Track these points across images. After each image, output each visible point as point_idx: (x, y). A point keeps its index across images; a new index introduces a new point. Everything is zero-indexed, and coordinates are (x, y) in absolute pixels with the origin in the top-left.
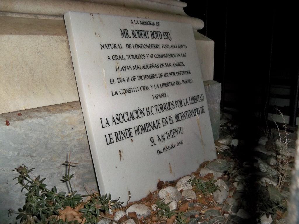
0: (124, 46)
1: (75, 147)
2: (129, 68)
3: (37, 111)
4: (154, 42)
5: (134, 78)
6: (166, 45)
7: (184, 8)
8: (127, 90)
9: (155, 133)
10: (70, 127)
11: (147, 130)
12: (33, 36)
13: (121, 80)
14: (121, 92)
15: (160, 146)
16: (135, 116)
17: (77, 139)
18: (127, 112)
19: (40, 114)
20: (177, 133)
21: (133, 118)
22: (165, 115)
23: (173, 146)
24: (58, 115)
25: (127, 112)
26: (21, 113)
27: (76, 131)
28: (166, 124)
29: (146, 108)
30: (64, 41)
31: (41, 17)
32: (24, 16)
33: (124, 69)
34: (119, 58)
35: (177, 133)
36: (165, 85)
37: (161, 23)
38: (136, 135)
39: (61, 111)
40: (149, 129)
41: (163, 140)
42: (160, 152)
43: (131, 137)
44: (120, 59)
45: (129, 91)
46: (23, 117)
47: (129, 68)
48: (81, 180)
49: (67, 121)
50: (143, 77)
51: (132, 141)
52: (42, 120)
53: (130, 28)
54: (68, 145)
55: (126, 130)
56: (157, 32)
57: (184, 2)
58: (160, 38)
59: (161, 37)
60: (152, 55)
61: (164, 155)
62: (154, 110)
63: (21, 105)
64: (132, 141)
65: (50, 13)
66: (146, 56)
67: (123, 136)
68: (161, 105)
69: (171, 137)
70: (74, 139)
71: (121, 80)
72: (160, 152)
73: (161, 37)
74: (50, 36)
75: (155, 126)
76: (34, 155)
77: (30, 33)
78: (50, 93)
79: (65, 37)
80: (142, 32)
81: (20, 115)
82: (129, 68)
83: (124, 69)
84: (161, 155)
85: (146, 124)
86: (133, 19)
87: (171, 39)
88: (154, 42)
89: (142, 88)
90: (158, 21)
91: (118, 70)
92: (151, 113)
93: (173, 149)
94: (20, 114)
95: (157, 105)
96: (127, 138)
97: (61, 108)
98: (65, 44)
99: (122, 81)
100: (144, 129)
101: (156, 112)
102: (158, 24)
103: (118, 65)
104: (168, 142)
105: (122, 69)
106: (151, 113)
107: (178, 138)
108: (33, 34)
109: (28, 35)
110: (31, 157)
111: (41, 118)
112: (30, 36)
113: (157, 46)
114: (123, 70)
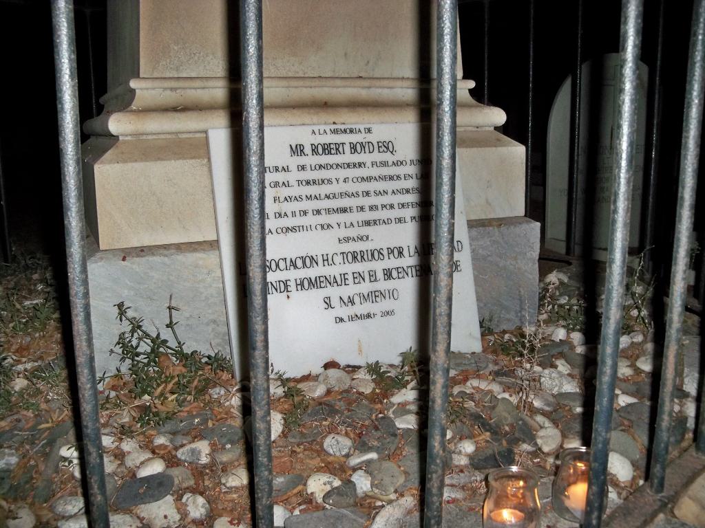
0: (293, 168)
1: (212, 296)
2: (298, 199)
3: (165, 248)
4: (356, 158)
5: (305, 213)
6: (381, 163)
7: (471, 91)
8: (290, 228)
9: (334, 292)
10: (205, 271)
11: (318, 285)
12: (163, 162)
13: (280, 215)
14: (279, 231)
15: (345, 312)
16: (299, 263)
17: (216, 287)
18: (285, 259)
19: (166, 252)
20: (385, 297)
21: (295, 267)
22: (351, 268)
23: (372, 316)
24: (189, 255)
25: (285, 259)
26: (145, 249)
27: (214, 277)
28: (361, 280)
29: (323, 255)
30: (203, 165)
31: (184, 136)
32: (162, 136)
33: (289, 200)
34: (281, 185)
35: (385, 297)
36: (368, 223)
37: (375, 128)
38: (297, 290)
39: (195, 250)
40: (323, 285)
41: (350, 304)
42: (342, 320)
43: (288, 291)
44: (284, 186)
45: (294, 230)
46: (145, 254)
47: (355, 195)
48: (221, 340)
49: (201, 263)
50: (323, 212)
51: (288, 297)
52: (166, 259)
53: (307, 139)
54: (201, 293)
55: (279, 281)
56: (364, 144)
57: (61, 179)
58: (370, 152)
59: (371, 150)
60: (347, 180)
61: (348, 325)
62: (338, 259)
63: (147, 241)
64: (288, 297)
65: (193, 130)
66: (334, 181)
67: (273, 289)
68: (354, 252)
69: (368, 301)
70: (211, 286)
71: (280, 215)
72: (342, 320)
73: (371, 150)
74: (185, 161)
75: (336, 282)
76: (155, 298)
77: (159, 159)
78: (184, 227)
79: (206, 160)
80: (332, 146)
81: (142, 251)
82: (298, 199)
83: (289, 200)
84: (341, 324)
85: (318, 278)
86: (316, 128)
87: (394, 153)
88: (356, 158)
89: (319, 227)
90: (368, 126)
91: (277, 202)
92: (330, 262)
93: (369, 320)
94: (142, 251)
95: (347, 252)
96: (281, 292)
97: (197, 247)
98: (206, 169)
99: (283, 216)
100: (314, 283)
101: (342, 262)
102: (369, 131)
103: (279, 195)
104: (360, 309)
105: (286, 199)
106: (330, 262)
107: (385, 305)
108: (162, 160)
109: (156, 161)
110: (151, 299)
111: (166, 256)
112: (159, 162)
113: (359, 165)
114: (286, 201)
